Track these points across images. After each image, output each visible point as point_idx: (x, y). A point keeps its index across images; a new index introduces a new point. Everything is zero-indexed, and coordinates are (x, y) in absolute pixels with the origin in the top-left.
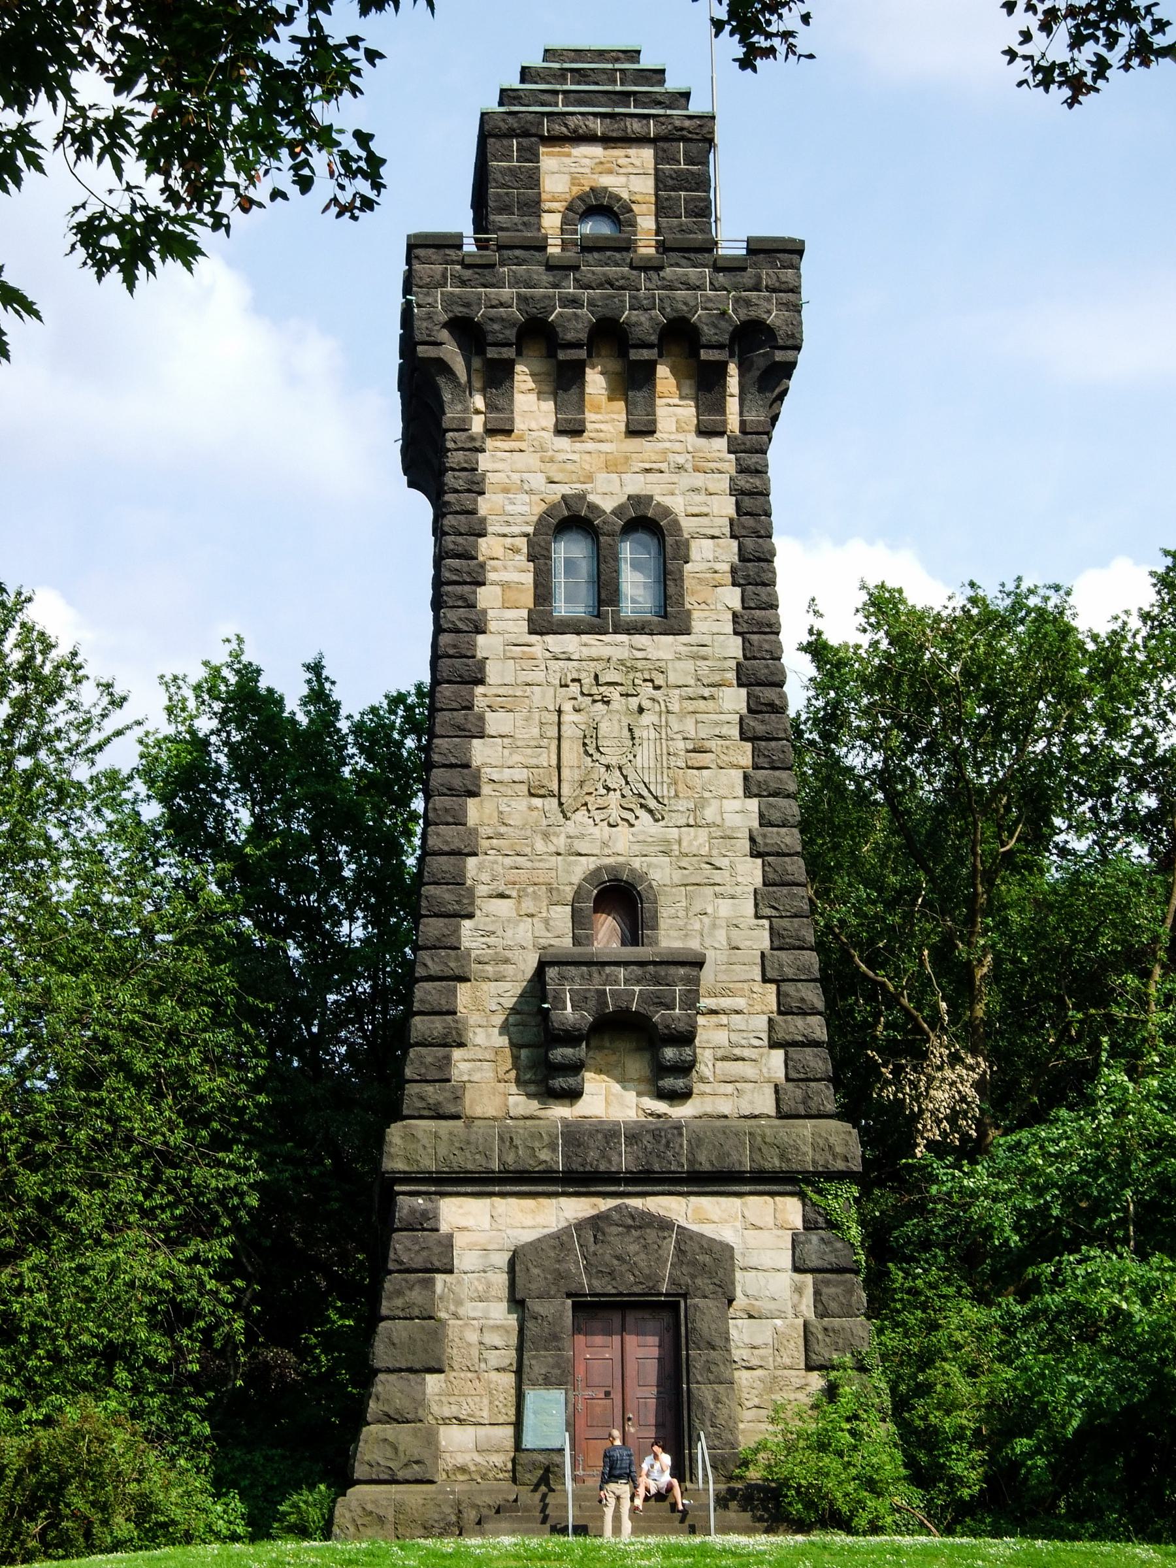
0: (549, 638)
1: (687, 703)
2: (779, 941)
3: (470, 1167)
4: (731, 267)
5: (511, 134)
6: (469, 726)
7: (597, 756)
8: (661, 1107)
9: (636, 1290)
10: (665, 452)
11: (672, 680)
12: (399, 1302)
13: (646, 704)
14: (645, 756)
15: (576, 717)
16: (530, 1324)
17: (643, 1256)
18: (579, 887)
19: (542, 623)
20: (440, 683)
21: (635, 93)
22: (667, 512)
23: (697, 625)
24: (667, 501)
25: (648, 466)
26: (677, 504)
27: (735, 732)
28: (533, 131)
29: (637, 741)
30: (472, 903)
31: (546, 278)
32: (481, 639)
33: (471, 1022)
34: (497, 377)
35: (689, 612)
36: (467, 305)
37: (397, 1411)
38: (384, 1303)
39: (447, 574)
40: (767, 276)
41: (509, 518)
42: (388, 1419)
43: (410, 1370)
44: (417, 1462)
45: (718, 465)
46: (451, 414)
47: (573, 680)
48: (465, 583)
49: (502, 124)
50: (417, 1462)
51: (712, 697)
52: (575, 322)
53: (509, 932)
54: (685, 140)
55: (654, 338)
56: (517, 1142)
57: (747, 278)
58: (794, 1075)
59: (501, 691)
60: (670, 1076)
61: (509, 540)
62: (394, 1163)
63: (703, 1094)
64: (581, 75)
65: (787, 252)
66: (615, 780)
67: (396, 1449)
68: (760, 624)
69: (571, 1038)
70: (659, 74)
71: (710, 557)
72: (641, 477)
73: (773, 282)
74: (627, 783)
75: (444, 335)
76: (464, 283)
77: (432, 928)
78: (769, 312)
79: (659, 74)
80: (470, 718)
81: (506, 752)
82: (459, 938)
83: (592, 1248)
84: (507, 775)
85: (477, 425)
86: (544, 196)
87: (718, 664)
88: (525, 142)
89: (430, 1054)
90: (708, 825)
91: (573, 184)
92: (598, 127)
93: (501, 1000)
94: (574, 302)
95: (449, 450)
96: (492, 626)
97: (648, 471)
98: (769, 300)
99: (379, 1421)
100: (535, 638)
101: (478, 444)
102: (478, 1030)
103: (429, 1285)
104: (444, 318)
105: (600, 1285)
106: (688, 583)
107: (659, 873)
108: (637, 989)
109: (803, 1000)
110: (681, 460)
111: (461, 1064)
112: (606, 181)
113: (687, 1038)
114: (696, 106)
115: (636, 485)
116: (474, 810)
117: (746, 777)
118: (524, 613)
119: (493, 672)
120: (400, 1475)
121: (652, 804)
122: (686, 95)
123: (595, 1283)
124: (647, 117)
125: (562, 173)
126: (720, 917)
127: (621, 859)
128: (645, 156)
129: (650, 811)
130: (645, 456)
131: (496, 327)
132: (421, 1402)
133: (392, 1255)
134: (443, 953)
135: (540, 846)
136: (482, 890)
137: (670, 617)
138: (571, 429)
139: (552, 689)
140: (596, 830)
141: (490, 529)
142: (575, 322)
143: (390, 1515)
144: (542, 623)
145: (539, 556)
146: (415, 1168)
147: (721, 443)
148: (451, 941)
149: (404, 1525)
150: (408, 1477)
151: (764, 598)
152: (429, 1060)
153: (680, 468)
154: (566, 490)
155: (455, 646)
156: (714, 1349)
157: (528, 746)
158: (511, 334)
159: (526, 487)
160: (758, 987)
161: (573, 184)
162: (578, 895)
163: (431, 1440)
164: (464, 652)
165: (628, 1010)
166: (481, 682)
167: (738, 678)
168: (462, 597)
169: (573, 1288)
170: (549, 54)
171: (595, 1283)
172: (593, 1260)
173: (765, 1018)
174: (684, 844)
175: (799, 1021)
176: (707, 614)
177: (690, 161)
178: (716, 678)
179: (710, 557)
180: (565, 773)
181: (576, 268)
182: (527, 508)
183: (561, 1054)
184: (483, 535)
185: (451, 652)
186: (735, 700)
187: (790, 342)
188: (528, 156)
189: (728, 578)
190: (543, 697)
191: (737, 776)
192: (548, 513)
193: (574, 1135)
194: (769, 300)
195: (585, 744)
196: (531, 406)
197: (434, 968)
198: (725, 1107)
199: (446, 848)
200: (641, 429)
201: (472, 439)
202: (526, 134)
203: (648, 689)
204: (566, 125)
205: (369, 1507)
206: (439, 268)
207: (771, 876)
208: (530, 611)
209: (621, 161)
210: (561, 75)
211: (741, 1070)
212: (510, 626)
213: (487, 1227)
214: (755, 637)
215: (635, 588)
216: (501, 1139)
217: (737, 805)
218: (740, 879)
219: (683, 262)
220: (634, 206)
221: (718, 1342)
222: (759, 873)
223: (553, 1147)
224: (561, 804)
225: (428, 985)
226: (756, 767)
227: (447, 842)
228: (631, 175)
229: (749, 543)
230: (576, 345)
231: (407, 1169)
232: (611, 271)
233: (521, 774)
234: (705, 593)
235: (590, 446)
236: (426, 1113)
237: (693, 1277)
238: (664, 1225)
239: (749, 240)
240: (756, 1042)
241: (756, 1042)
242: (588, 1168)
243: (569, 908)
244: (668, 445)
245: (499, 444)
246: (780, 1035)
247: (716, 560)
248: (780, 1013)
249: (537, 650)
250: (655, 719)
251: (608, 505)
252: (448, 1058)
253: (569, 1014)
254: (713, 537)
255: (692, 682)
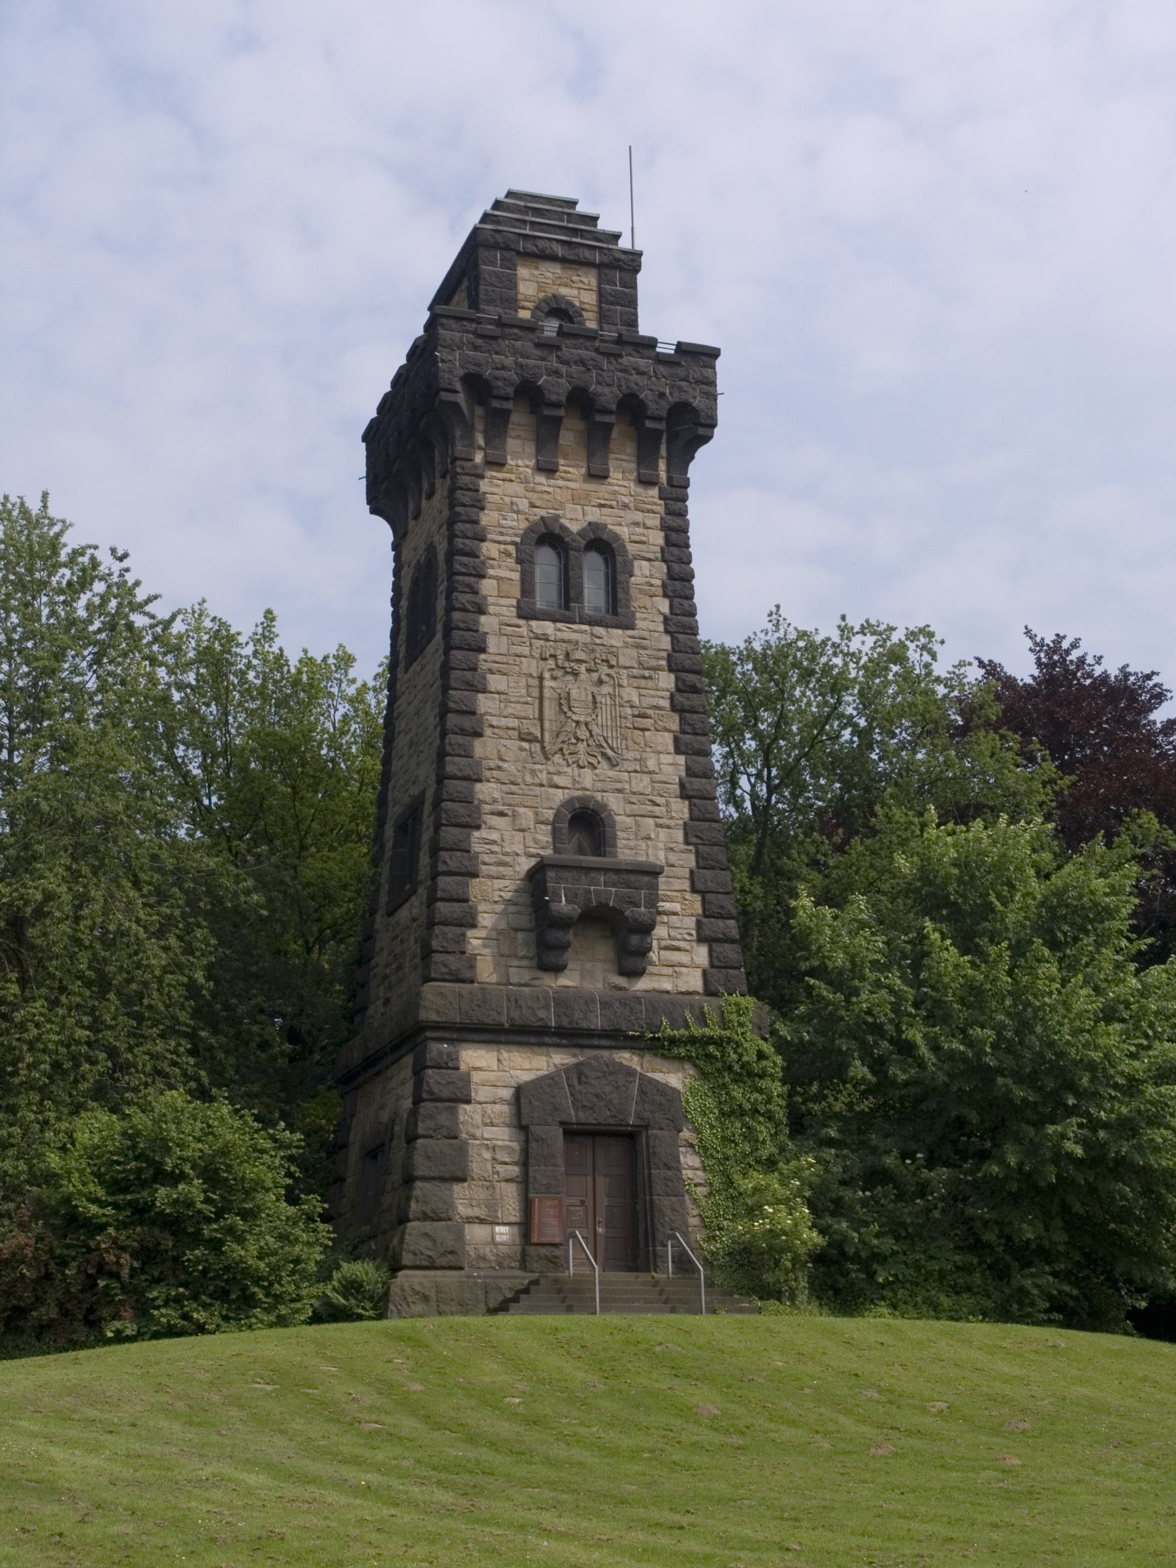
0: (533, 623)
1: (632, 680)
2: (703, 862)
3: (486, 1020)
4: (662, 360)
5: (496, 246)
6: (475, 683)
7: (569, 714)
8: (622, 981)
9: (611, 1121)
10: (615, 493)
11: (622, 661)
12: (431, 1124)
13: (604, 678)
14: (604, 716)
15: (553, 684)
16: (533, 1145)
17: (615, 1095)
18: (558, 811)
19: (526, 612)
20: (452, 648)
21: (582, 230)
22: (617, 537)
23: (640, 624)
24: (617, 529)
25: (603, 502)
26: (624, 532)
27: (666, 703)
28: (513, 246)
29: (599, 705)
30: (479, 818)
31: (538, 352)
32: (483, 619)
33: (480, 908)
34: (498, 424)
35: (633, 613)
36: (478, 365)
37: (433, 1211)
38: (420, 1124)
39: (458, 567)
40: (696, 372)
41: (503, 530)
42: (425, 1217)
43: (443, 1179)
44: (452, 1252)
45: (654, 507)
46: (459, 449)
47: (551, 656)
48: (470, 575)
49: (490, 238)
50: (452, 1252)
51: (650, 678)
52: (558, 389)
53: (507, 844)
54: (621, 269)
55: (614, 407)
56: (521, 1002)
57: (681, 372)
58: (716, 963)
59: (498, 658)
60: (631, 961)
61: (502, 546)
62: (428, 1014)
63: (652, 974)
64: (538, 212)
65: (714, 353)
66: (583, 733)
67: (434, 1241)
68: (684, 626)
69: (564, 923)
70: (594, 219)
71: (646, 574)
72: (597, 510)
73: (698, 375)
74: (591, 735)
75: (458, 386)
76: (476, 348)
77: (450, 834)
78: (695, 398)
79: (594, 219)
80: (477, 677)
81: (502, 705)
82: (470, 844)
83: (578, 1087)
84: (503, 722)
85: (479, 458)
86: (520, 297)
87: (655, 653)
88: (507, 254)
89: (452, 931)
90: (650, 773)
91: (540, 290)
92: (560, 251)
93: (502, 894)
94: (557, 373)
95: (458, 474)
96: (491, 609)
97: (603, 506)
98: (694, 389)
99: (419, 1219)
100: (522, 622)
101: (480, 471)
102: (485, 915)
103: (454, 1112)
104: (461, 372)
105: (584, 1116)
106: (633, 591)
107: (614, 803)
108: (613, 890)
109: (722, 907)
110: (626, 500)
111: (475, 940)
112: (564, 291)
113: (647, 929)
114: (624, 243)
115: (594, 515)
116: (480, 748)
117: (676, 739)
118: (514, 602)
119: (492, 644)
120: (439, 1262)
121: (610, 753)
122: (616, 237)
123: (581, 1114)
124: (594, 247)
125: (533, 283)
126: (655, 835)
127: (587, 793)
128: (590, 279)
129: (608, 759)
130: (601, 494)
131: (500, 384)
132: (451, 1205)
133: (425, 1087)
134: (459, 854)
135: (528, 779)
136: (487, 808)
137: (617, 611)
138: (549, 470)
139: (535, 661)
140: (569, 770)
141: (489, 536)
142: (558, 389)
143: (433, 1295)
144: (526, 612)
145: (525, 562)
146: (444, 1019)
147: (654, 492)
148: (464, 846)
149: (439, 1304)
150: (444, 1264)
151: (687, 608)
152: (450, 935)
153: (626, 506)
154: (543, 513)
155: (464, 622)
156: (669, 1169)
157: (519, 702)
158: (510, 391)
159: (515, 508)
160: (688, 896)
161: (540, 290)
162: (557, 815)
163: (460, 1236)
164: (471, 627)
165: (607, 905)
166: (483, 650)
167: (669, 665)
168: (469, 586)
169: (565, 1118)
170: (510, 194)
171: (581, 1114)
172: (579, 1097)
173: (694, 919)
174: (633, 784)
175: (720, 923)
176: (646, 616)
177: (624, 285)
178: (653, 663)
179: (646, 574)
180: (547, 724)
181: (558, 348)
182: (515, 524)
183: (554, 935)
184: (483, 540)
185: (462, 625)
186: (667, 681)
187: (708, 422)
188: (508, 264)
189: (660, 591)
190: (531, 666)
191: (668, 738)
192: (530, 530)
193: (562, 1000)
194: (694, 389)
195: (560, 704)
196: (520, 456)
197: (453, 865)
198: (667, 985)
199: (459, 774)
200: (598, 476)
201: (476, 467)
202: (507, 248)
203: (605, 669)
204: (536, 246)
205: (417, 1288)
206: (458, 335)
207: (696, 812)
208: (518, 601)
209: (574, 278)
210: (519, 210)
211: (679, 963)
212: (504, 610)
213: (495, 1068)
214: (680, 636)
215: (593, 593)
216: (509, 1000)
217: (669, 759)
218: (674, 814)
219: (634, 353)
220: (584, 313)
221: (672, 1164)
222: (686, 811)
223: (546, 1007)
224: (543, 748)
225: (449, 879)
226: (683, 732)
227: (460, 770)
228: (581, 290)
229: (675, 566)
230: (557, 405)
231: (438, 1019)
232: (584, 353)
233: (514, 723)
234: (646, 601)
235: (561, 483)
236: (447, 977)
237: (652, 1112)
238: (630, 1072)
239: (679, 344)
240: (688, 938)
241: (688, 938)
242: (574, 1025)
243: (549, 827)
244: (617, 488)
245: (494, 474)
246: (707, 933)
247: (651, 576)
248: (706, 916)
249: (524, 631)
250: (610, 690)
251: (575, 528)
252: (464, 935)
253: (563, 906)
254: (649, 560)
255: (636, 665)
